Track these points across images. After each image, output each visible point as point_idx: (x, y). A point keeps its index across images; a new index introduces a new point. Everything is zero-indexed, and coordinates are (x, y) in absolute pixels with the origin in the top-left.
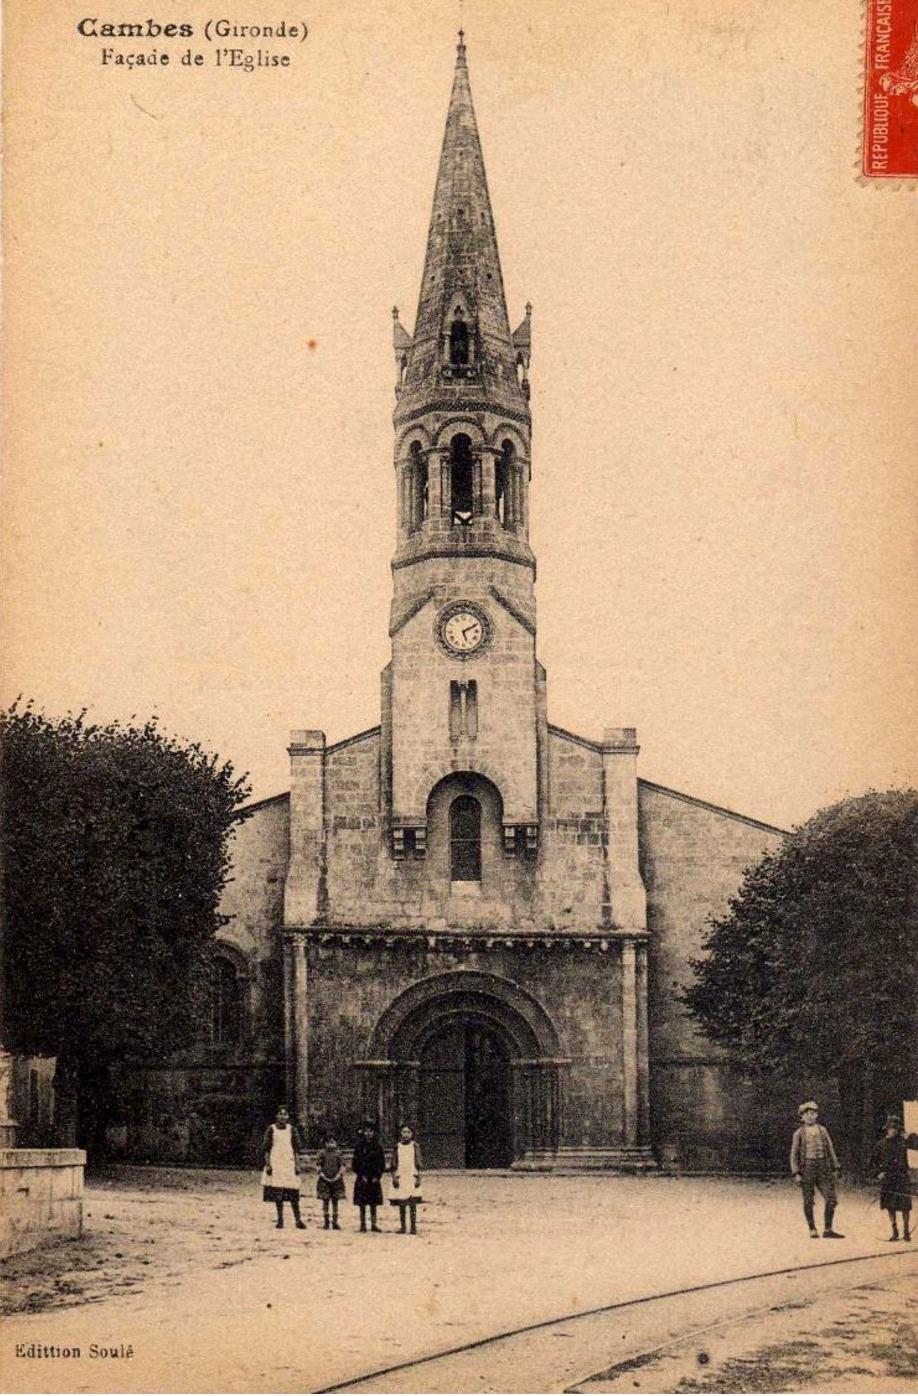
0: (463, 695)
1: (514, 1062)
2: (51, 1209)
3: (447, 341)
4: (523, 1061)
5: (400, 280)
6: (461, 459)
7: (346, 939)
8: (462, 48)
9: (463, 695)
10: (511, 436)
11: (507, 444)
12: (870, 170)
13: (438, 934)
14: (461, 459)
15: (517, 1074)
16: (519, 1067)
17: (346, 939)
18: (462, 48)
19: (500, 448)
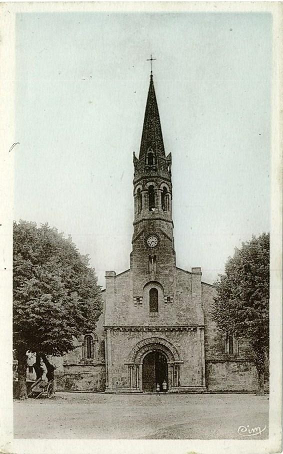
0: (153, 260)
1: (168, 363)
2: (27, 309)
3: (147, 159)
4: (170, 362)
5: (133, 143)
6: (151, 192)
7: (121, 329)
8: (152, 76)
9: (153, 260)
10: (166, 186)
11: (164, 188)
12: (15, 225)
13: (146, 327)
14: (151, 192)
15: (169, 365)
16: (169, 364)
17: (121, 329)
18: (152, 76)
19: (162, 189)
